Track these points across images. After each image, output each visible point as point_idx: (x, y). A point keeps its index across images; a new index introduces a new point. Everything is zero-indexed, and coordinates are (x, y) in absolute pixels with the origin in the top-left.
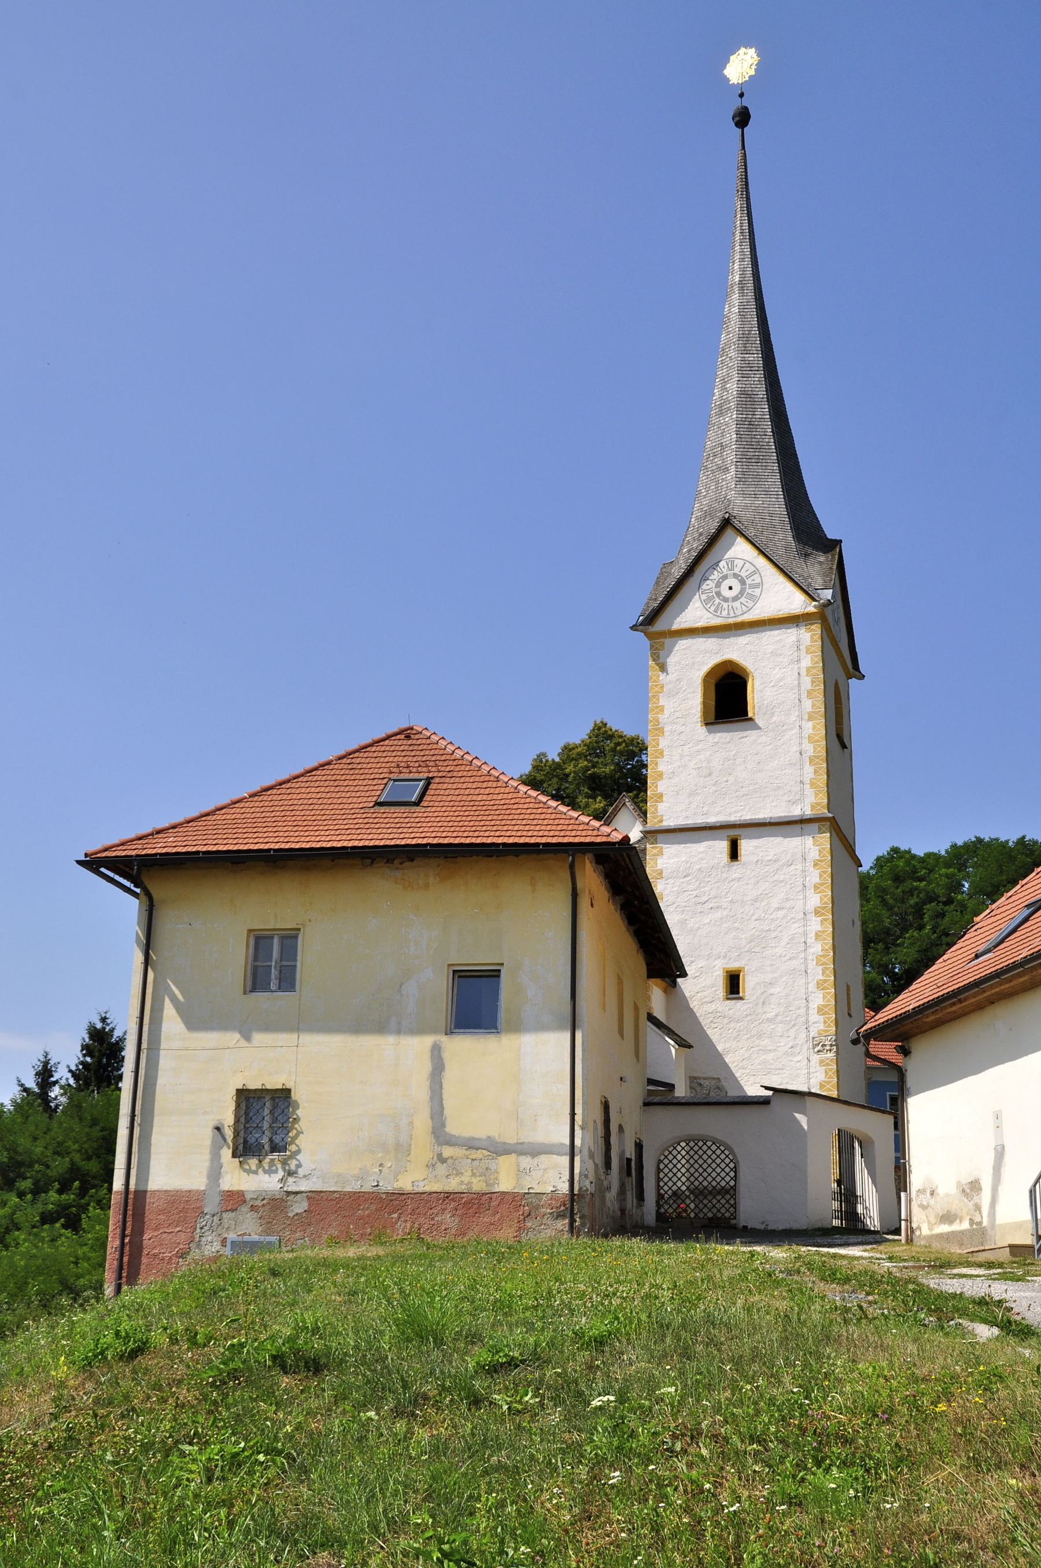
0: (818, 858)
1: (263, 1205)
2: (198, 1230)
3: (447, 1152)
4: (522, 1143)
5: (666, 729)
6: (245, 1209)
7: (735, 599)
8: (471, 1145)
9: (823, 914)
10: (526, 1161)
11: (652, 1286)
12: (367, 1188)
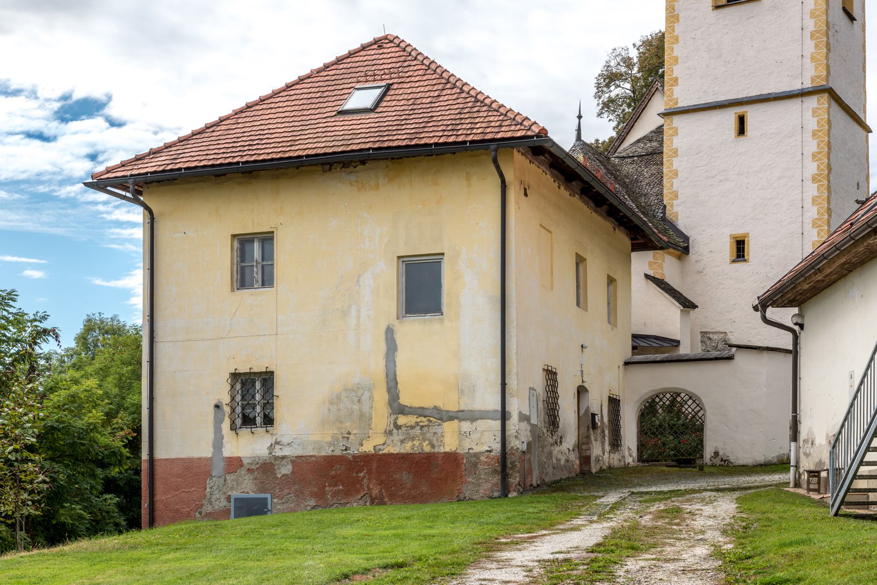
0: (816, 128)
1: (257, 468)
2: (208, 490)
3: (402, 420)
4: (462, 411)
5: (680, 16)
6: (243, 472)
8: (420, 412)
9: (820, 181)
10: (466, 426)
11: (797, 485)
12: (338, 453)
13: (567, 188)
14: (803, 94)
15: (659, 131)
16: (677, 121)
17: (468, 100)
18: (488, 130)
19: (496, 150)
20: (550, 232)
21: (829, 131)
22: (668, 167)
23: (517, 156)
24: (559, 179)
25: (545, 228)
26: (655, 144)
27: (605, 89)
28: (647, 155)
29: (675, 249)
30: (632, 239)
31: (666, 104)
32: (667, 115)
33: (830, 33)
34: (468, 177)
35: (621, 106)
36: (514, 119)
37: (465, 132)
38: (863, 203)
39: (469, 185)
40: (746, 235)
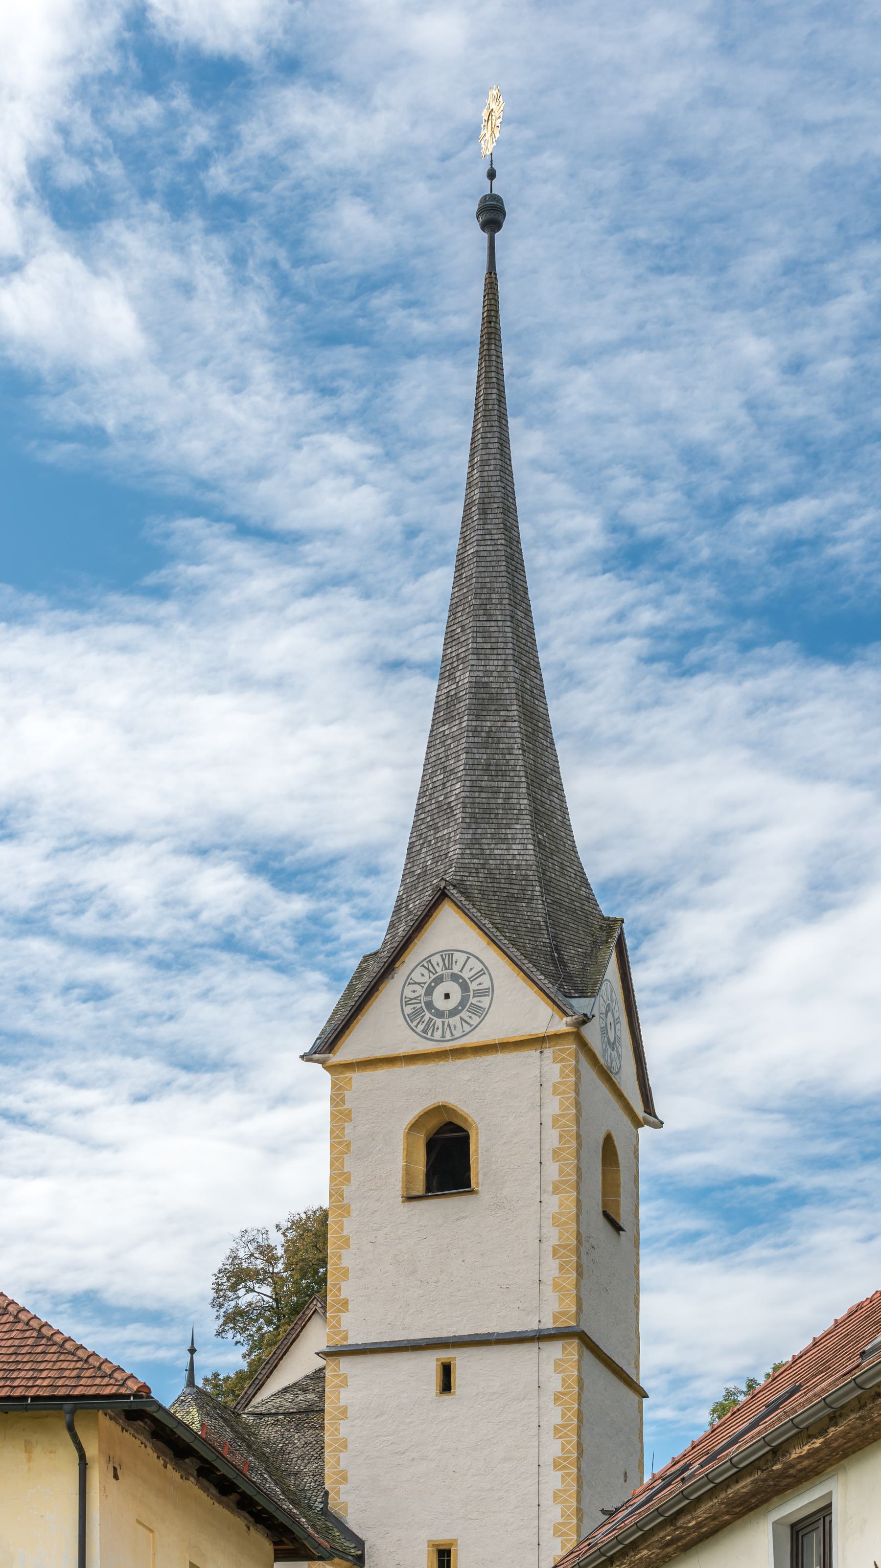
0: (560, 1389)
5: (352, 1207)
7: (453, 1013)
9: (565, 1467)
13: (177, 1467)
14: (540, 1337)
15: (318, 1376)
16: (346, 1365)
17: (28, 1334)
18: (60, 1382)
19: (72, 1412)
20: (152, 1531)
21: (579, 1395)
22: (332, 1434)
23: (104, 1421)
24: (165, 1455)
25: (144, 1526)
26: (311, 1396)
27: (229, 1294)
28: (299, 1413)
29: (342, 1558)
30: (275, 1543)
31: (330, 1338)
32: (332, 1354)
33: (583, 1250)
34: (28, 1448)
35: (256, 1321)
36: (99, 1368)
37: (24, 1383)
38: (611, 1514)
39: (29, 1460)
40: (454, 1542)
